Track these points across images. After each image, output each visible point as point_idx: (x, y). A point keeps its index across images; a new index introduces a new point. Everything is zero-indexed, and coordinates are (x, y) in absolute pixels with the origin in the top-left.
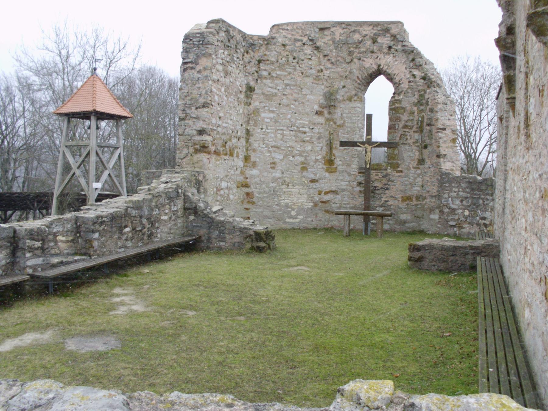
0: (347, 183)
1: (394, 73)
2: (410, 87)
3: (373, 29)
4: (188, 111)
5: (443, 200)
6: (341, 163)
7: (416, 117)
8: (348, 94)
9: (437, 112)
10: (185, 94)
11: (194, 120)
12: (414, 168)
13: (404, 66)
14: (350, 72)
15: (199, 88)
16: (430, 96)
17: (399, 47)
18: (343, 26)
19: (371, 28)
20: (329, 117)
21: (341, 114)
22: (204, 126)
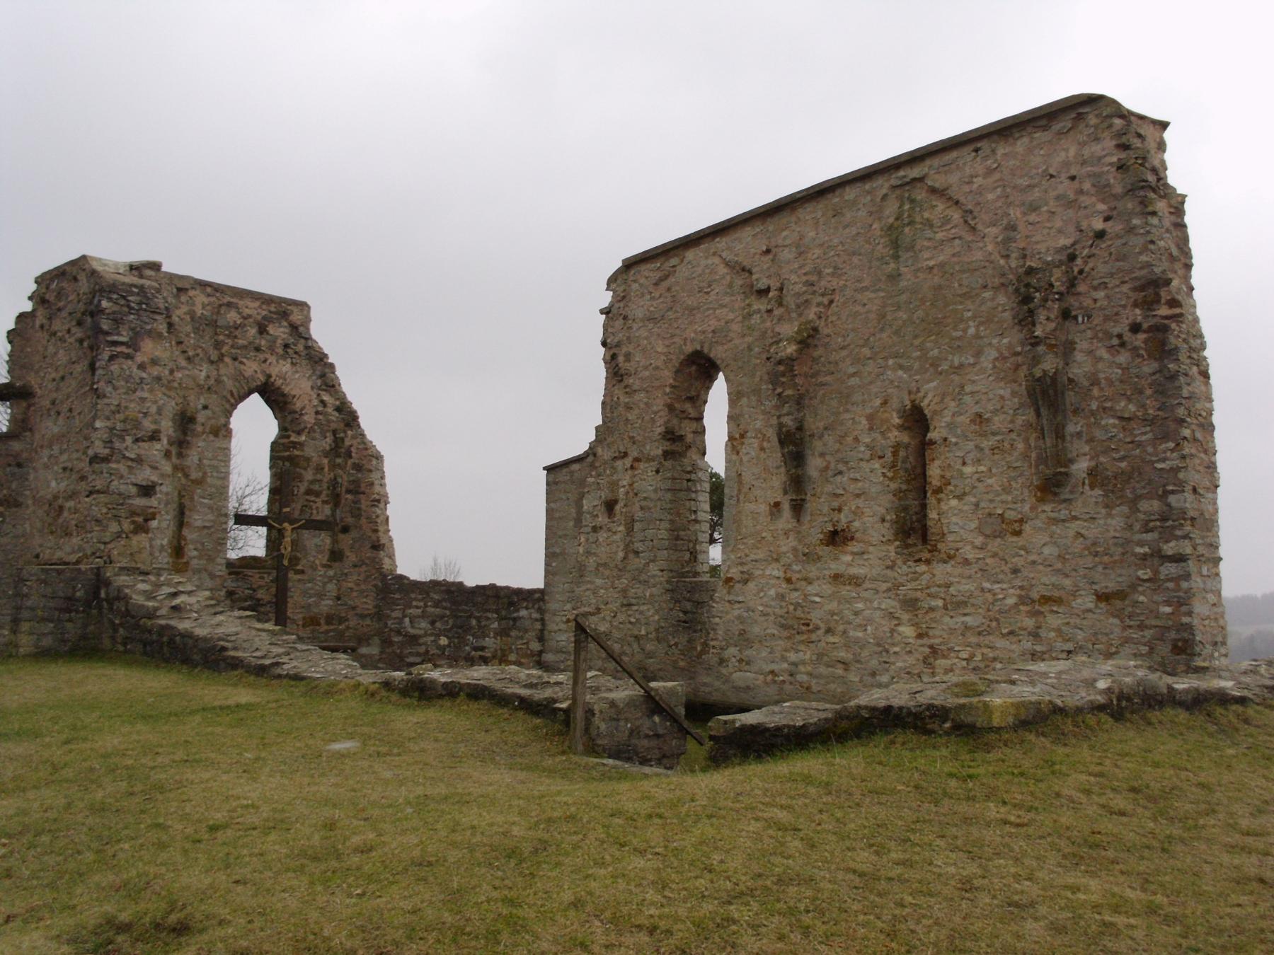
0: (207, 593)
1: (293, 393)
2: (318, 423)
3: (260, 307)
4: (117, 445)
5: (389, 623)
6: (195, 553)
7: (327, 476)
8: (213, 421)
9: (370, 471)
10: (113, 408)
11: (130, 463)
12: (324, 566)
13: (310, 384)
14: (218, 381)
15: (143, 400)
16: (355, 442)
17: (300, 347)
18: (209, 290)
19: (257, 304)
20: (178, 462)
21: (200, 460)
22: (154, 478)
